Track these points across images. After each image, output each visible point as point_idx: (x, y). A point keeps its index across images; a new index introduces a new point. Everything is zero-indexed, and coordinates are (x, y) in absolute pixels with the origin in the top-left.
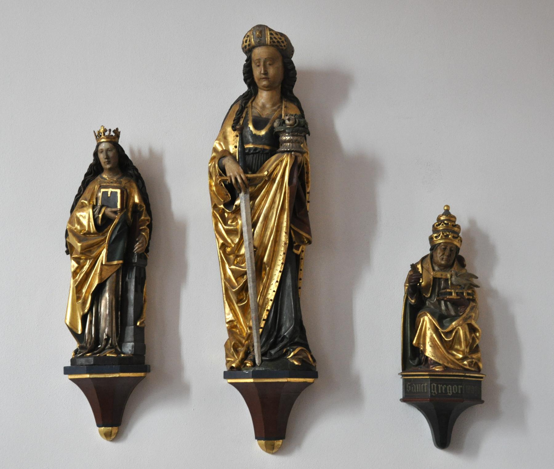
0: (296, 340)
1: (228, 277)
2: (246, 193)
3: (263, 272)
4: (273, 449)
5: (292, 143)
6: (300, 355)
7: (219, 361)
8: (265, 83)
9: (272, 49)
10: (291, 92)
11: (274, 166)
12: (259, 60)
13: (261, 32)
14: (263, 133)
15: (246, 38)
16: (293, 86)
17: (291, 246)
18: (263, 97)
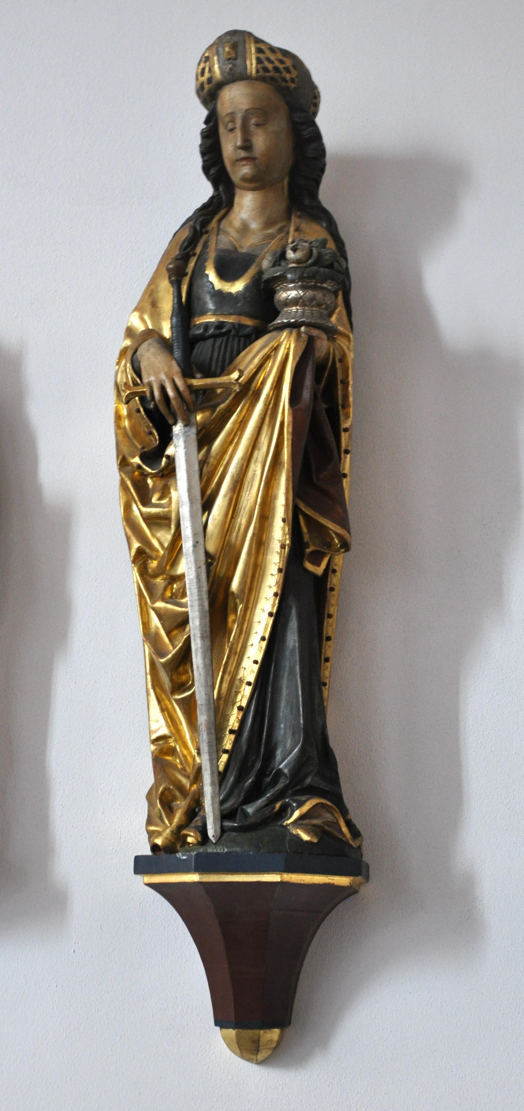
0: (308, 781)
1: (153, 630)
2: (187, 424)
3: (231, 618)
4: (257, 1050)
5: (304, 305)
6: (317, 817)
7: (134, 833)
8: (246, 170)
9: (261, 88)
10: (314, 194)
11: (256, 361)
12: (232, 115)
13: (234, 46)
14: (238, 287)
15: (202, 65)
16: (317, 182)
17: (296, 554)
18: (246, 205)
